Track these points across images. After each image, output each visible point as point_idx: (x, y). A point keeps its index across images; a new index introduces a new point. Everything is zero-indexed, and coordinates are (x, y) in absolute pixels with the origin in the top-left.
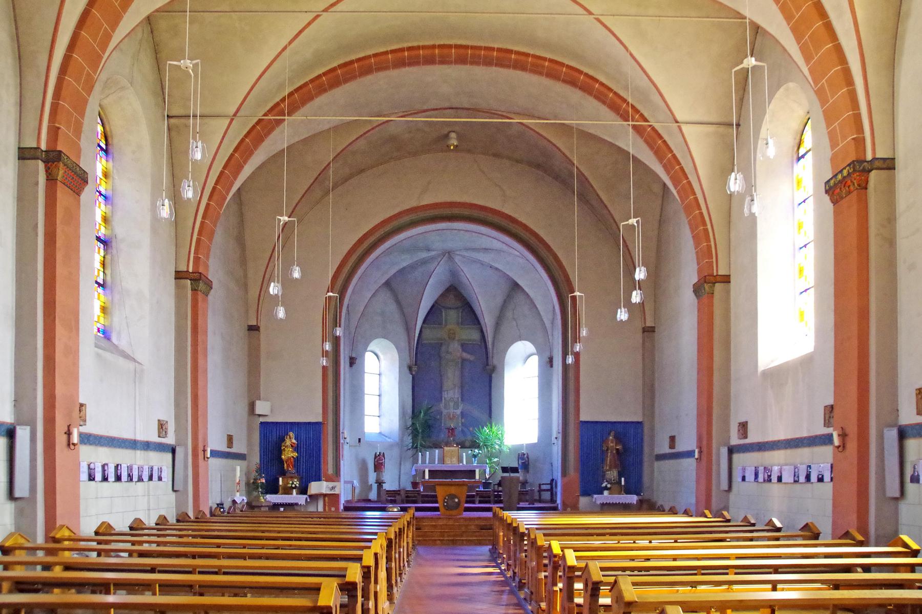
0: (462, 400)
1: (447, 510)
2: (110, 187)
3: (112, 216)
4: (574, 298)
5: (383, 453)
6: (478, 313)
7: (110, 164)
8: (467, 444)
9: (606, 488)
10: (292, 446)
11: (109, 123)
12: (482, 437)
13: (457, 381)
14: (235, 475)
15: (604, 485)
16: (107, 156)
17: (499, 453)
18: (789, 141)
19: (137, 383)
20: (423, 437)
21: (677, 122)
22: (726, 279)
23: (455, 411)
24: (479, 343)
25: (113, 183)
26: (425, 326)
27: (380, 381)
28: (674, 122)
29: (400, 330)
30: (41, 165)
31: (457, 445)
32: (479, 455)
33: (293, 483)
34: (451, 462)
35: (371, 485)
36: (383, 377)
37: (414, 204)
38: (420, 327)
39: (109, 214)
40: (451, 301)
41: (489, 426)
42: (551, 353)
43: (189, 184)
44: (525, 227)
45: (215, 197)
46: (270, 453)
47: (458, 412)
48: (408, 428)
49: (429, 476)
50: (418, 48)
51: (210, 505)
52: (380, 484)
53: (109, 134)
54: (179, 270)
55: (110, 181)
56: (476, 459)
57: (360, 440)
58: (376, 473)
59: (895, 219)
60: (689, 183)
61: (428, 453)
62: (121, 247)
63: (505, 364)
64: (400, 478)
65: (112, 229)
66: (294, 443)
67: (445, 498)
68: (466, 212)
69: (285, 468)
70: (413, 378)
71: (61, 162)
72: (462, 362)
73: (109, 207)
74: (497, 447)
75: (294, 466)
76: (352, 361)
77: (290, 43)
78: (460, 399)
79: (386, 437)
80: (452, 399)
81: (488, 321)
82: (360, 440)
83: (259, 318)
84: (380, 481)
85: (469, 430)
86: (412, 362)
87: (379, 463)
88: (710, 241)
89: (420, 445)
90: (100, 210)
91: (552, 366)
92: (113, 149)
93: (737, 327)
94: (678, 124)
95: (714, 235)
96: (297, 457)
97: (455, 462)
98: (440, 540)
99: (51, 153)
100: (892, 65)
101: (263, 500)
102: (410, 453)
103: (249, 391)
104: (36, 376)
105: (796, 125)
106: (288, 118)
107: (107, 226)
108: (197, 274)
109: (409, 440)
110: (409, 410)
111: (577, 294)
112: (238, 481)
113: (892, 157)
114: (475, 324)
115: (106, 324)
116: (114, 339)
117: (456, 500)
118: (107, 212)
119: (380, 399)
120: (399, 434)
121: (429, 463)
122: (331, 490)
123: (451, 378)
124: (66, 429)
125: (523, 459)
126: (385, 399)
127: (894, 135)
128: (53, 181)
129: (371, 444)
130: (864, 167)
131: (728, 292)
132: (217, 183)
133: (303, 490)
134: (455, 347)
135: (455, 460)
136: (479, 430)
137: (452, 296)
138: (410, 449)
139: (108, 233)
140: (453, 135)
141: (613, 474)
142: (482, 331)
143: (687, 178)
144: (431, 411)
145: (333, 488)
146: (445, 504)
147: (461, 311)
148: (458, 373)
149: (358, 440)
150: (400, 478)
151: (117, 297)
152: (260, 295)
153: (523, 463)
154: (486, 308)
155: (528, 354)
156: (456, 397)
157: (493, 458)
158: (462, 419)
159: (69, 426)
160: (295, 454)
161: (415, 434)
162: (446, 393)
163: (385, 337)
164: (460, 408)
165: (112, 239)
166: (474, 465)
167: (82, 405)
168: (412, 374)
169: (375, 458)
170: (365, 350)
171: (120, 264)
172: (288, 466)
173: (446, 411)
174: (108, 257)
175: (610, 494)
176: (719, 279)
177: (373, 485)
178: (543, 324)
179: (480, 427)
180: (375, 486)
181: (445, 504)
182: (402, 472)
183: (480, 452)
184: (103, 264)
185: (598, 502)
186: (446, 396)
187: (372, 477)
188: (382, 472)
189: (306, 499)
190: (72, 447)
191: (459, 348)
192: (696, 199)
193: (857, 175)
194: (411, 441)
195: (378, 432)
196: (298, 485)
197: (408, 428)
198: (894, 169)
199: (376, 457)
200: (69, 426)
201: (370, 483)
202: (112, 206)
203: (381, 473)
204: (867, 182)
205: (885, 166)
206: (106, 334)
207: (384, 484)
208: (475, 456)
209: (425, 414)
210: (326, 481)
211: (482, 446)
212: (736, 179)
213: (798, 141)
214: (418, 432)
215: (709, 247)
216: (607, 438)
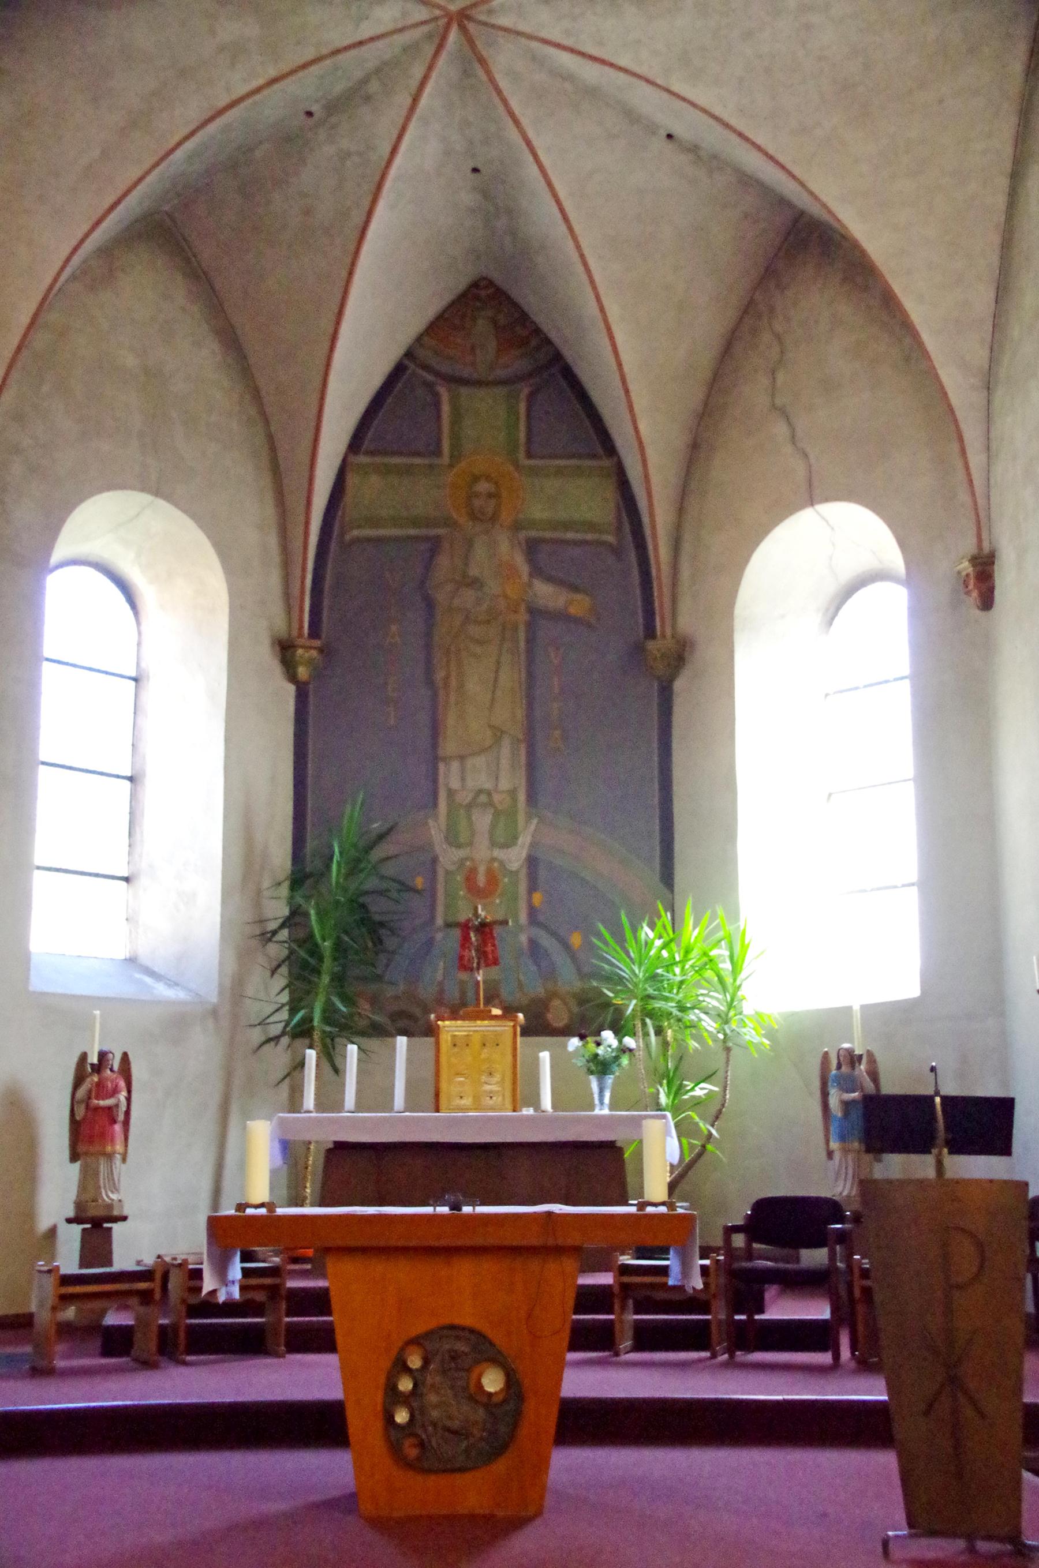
0: (532, 798)
1: (409, 1465)
5: (125, 1057)
17: (722, 1056)
20: (339, 980)
23: (497, 853)
24: (610, 538)
31: (509, 1012)
32: (625, 1061)
34: (477, 1098)
38: (337, 462)
41: (666, 918)
46: (465, 1033)
47: (515, 857)
48: (267, 937)
49: (192, 1269)
56: (610, 1080)
58: (77, 1166)
61: (352, 1049)
63: (738, 624)
67: (401, 1366)
72: (531, 627)
74: (709, 1024)
78: (522, 797)
80: (483, 798)
84: (93, 1212)
85: (566, 946)
86: (295, 625)
87: (97, 1108)
89: (327, 1020)
91: (987, 602)
97: (497, 1100)
102: (279, 1057)
114: (594, 456)
117: (492, 1382)
119: (134, 796)
120: (221, 964)
121: (359, 1107)
125: (848, 1083)
135: (495, 1086)
136: (621, 941)
137: (482, 326)
138: (276, 1039)
142: (623, 485)
144: (377, 854)
147: (526, 391)
148: (510, 677)
155: (848, 571)
156: (505, 784)
157: (689, 1085)
162: (455, 765)
164: (525, 840)
166: (597, 1112)
169: (79, 1080)
183: (629, 1042)
186: (455, 784)
194: (285, 998)
195: (122, 954)
197: (267, 937)
201: (44, 1224)
203: (102, 1161)
207: (117, 1228)
208: (601, 1067)
209: (354, 867)
211: (633, 1015)
214: (315, 951)
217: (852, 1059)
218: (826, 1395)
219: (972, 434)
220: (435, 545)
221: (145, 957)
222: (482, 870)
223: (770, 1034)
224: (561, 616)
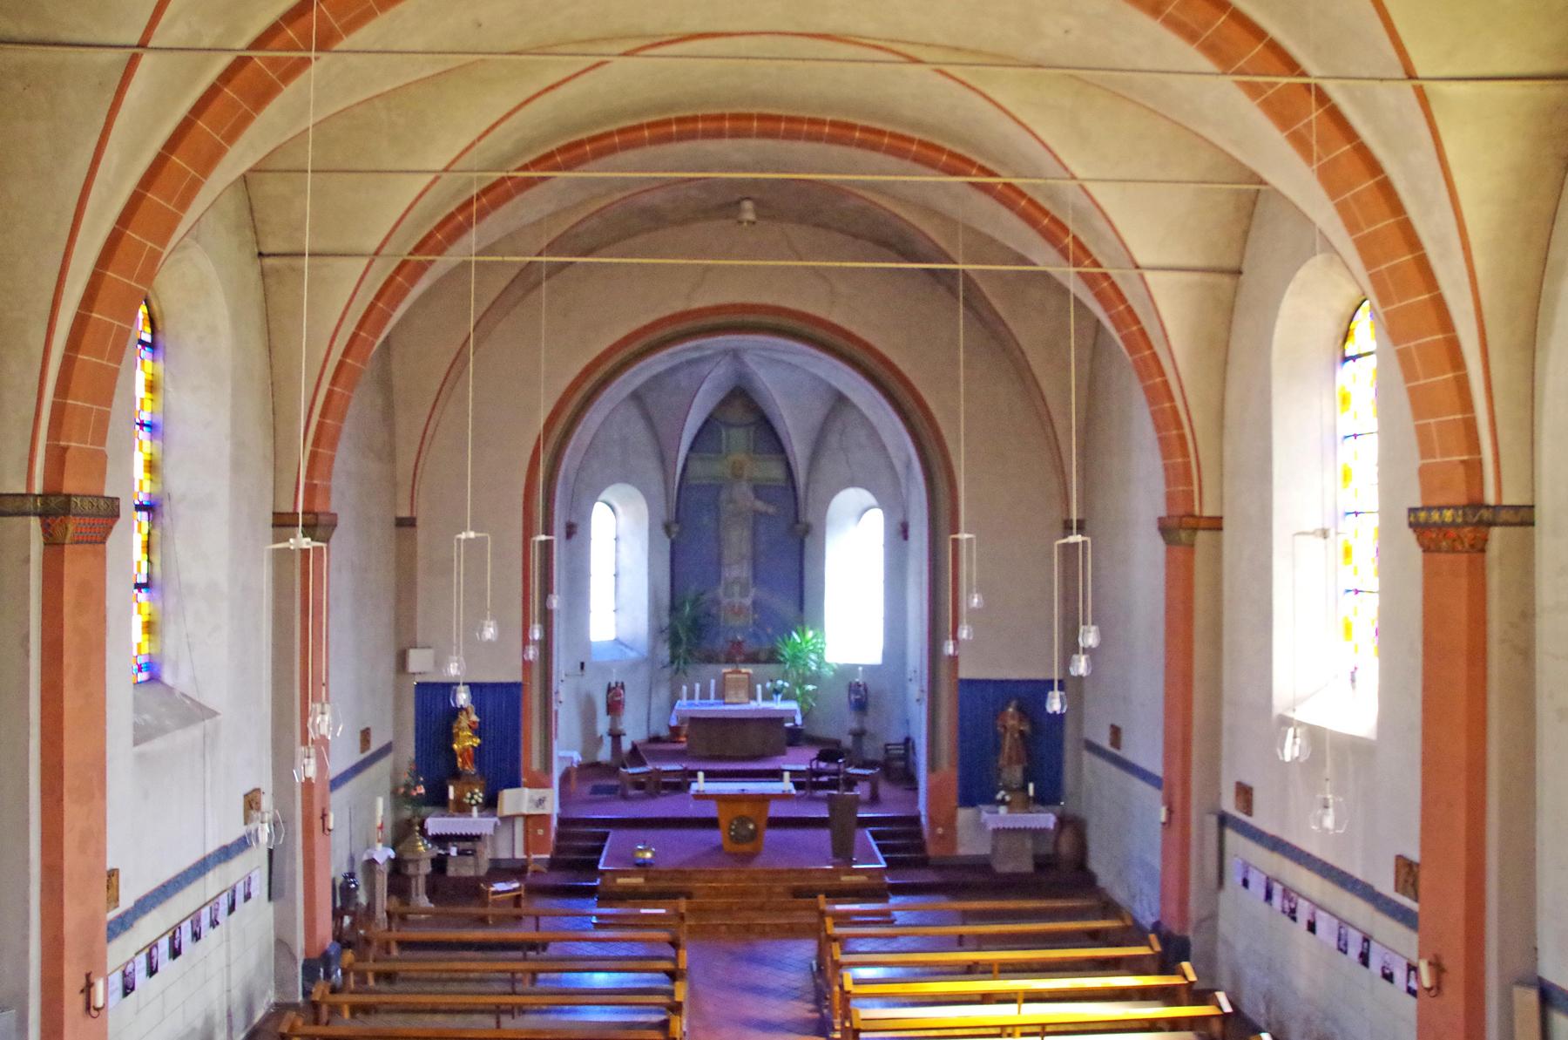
0: (754, 582)
2: (159, 408)
3: (163, 460)
4: (956, 541)
6: (782, 434)
7: (160, 366)
8: (763, 656)
9: (1002, 802)
10: (470, 727)
11: (157, 297)
12: (787, 652)
13: (746, 548)
14: (374, 818)
15: (999, 796)
16: (153, 354)
18: (1328, 328)
19: (208, 757)
21: (1137, 267)
22: (1216, 524)
25: (164, 398)
26: (693, 455)
27: (617, 551)
28: (1131, 266)
29: (651, 468)
30: (35, 523)
33: (472, 798)
35: (601, 737)
36: (623, 547)
37: (679, 306)
39: (158, 456)
40: (736, 413)
42: (904, 515)
43: (309, 753)
44: (867, 347)
45: (343, 379)
47: (748, 602)
50: (695, 119)
51: (333, 874)
52: (616, 736)
53: (157, 315)
54: (282, 511)
55: (160, 400)
57: (582, 665)
59: (1534, 615)
60: (1155, 356)
62: (179, 516)
64: (649, 719)
65: (163, 483)
66: (474, 723)
67: (732, 824)
68: (770, 320)
69: (459, 765)
70: (673, 544)
71: (71, 516)
73: (158, 442)
75: (475, 762)
76: (571, 530)
77: (480, 138)
79: (626, 646)
80: (737, 580)
81: (798, 450)
82: (582, 665)
83: (416, 487)
88: (1191, 483)
90: (143, 449)
91: (906, 537)
92: (166, 340)
93: (1235, 615)
94: (1139, 271)
95: (1190, 420)
96: (480, 745)
98: (725, 924)
99: (52, 498)
100: (1531, 343)
101: (422, 848)
103: (398, 633)
104: (27, 912)
105: (1341, 305)
106: (470, 258)
107: (153, 478)
108: (311, 516)
109: (665, 652)
110: (665, 600)
111: (963, 536)
112: (379, 823)
113: (1530, 504)
115: (153, 651)
116: (167, 677)
118: (154, 451)
122: (537, 806)
123: (737, 540)
124: (83, 982)
125: (857, 692)
126: (624, 580)
127: (1533, 473)
128: (56, 547)
129: (603, 668)
130: (1481, 516)
131: (1218, 547)
132: (346, 353)
133: (491, 804)
134: (743, 495)
136: (783, 640)
139: (157, 489)
140: (748, 205)
141: (1015, 774)
143: (1150, 347)
145: (541, 802)
146: (732, 833)
148: (746, 533)
149: (579, 664)
150: (649, 719)
151: (171, 601)
152: (416, 466)
153: (856, 700)
154: (795, 427)
158: (754, 614)
159: (88, 976)
160: (477, 741)
161: (675, 641)
163: (625, 479)
165: (162, 499)
167: (113, 874)
168: (669, 536)
170: (594, 499)
171: (176, 541)
172: (464, 763)
173: (728, 600)
174: (156, 533)
175: (1009, 812)
176: (1203, 523)
177: (604, 738)
178: (892, 467)
179: (785, 635)
180: (608, 741)
181: (732, 833)
182: (653, 707)
184: (148, 547)
185: (991, 826)
187: (603, 724)
188: (619, 715)
189: (496, 825)
190: (94, 1013)
191: (751, 494)
192: (1166, 383)
193: (1469, 532)
195: (612, 637)
196: (480, 800)
198: (1532, 524)
199: (609, 690)
200: (88, 976)
201: (599, 735)
202: (163, 442)
204: (1485, 540)
205: (1518, 519)
206: (152, 671)
210: (529, 786)
212: (1295, 737)
213: (1344, 329)
215: (1187, 466)
216: (1003, 710)
217: (858, 685)
218: (948, 617)
219: (903, 481)
220: (719, 488)
221: (622, 638)
222: (737, 606)
223: (834, 670)
224: (766, 514)
